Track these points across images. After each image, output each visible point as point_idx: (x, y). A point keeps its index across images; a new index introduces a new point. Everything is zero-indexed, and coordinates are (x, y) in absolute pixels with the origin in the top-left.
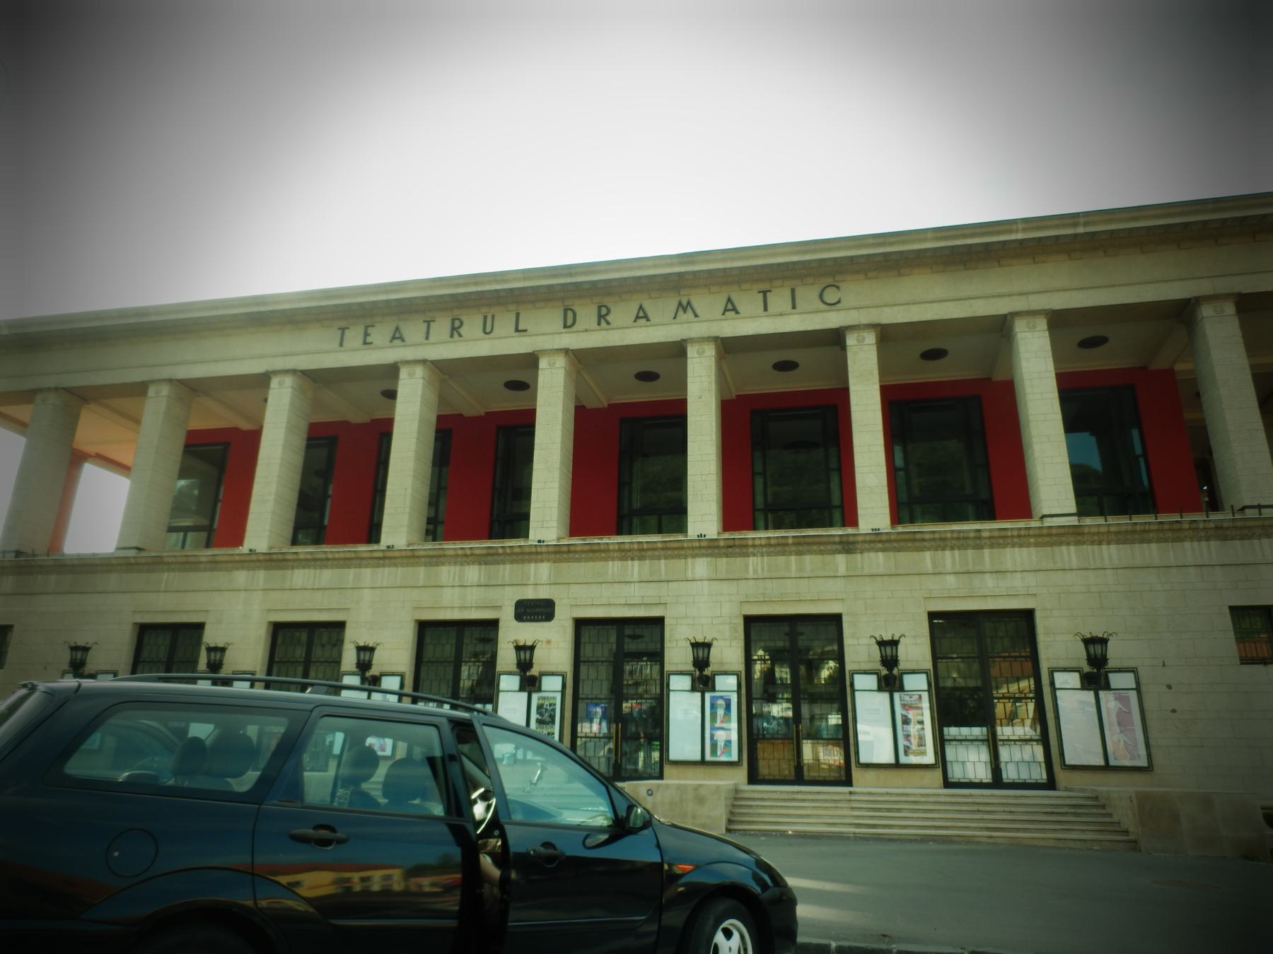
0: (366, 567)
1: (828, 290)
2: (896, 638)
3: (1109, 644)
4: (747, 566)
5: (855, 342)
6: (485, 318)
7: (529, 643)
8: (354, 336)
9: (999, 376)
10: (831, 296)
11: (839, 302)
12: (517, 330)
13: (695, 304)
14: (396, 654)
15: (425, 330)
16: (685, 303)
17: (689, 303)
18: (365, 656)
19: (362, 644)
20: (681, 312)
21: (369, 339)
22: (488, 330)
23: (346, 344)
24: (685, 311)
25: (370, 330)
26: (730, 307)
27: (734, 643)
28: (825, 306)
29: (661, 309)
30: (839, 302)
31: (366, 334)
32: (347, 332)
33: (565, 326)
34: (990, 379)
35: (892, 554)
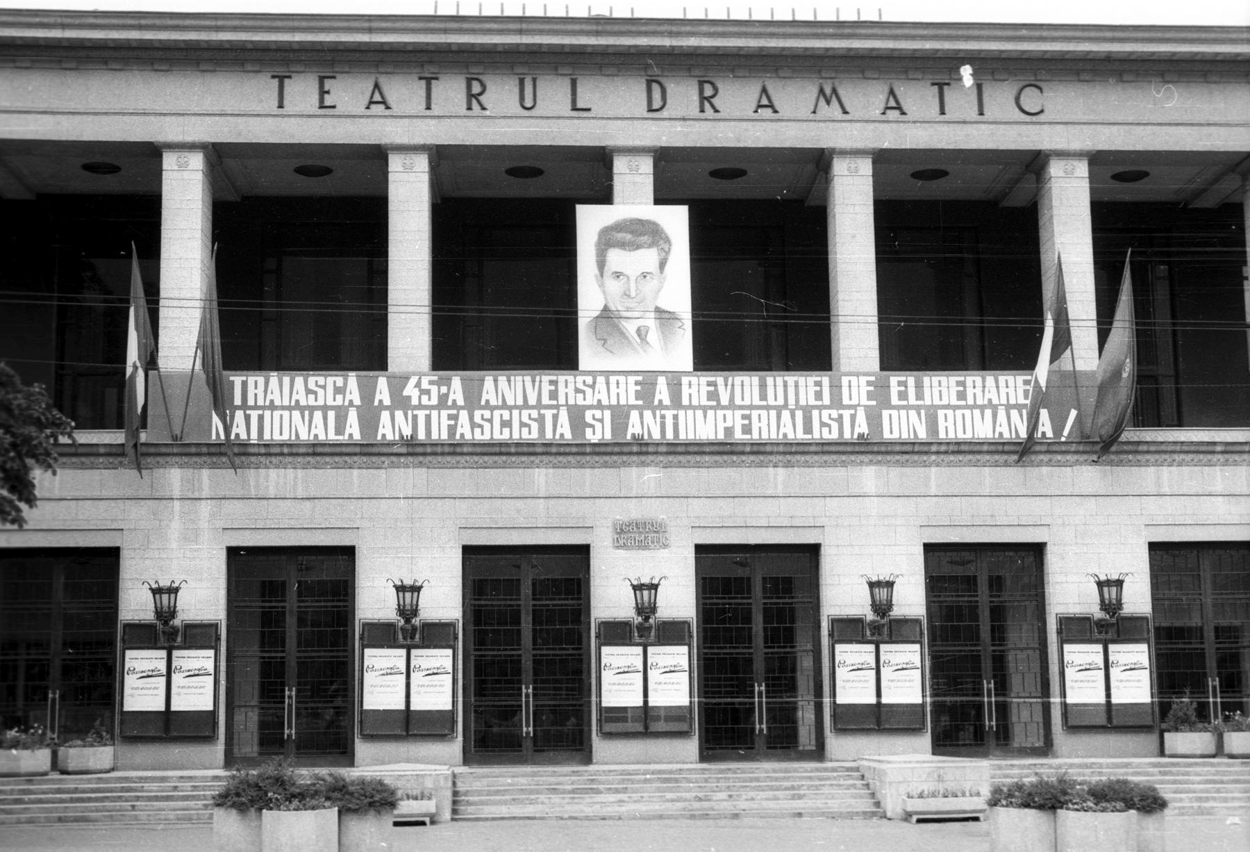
0: (172, 466)
1: (1028, 89)
2: (655, 582)
3: (1125, 585)
4: (928, 478)
5: (1061, 174)
6: (522, 82)
7: (1115, 577)
8: (302, 91)
9: (812, 202)
10: (1031, 100)
11: (1042, 111)
12: (574, 109)
13: (841, 92)
14: (205, 598)
15: (423, 93)
16: (828, 91)
17: (834, 91)
18: (882, 594)
19: (874, 579)
20: (822, 102)
21: (328, 100)
22: (528, 104)
23: (289, 108)
24: (828, 102)
25: (328, 84)
26: (892, 103)
27: (912, 580)
28: (1028, 118)
29: (795, 97)
30: (1042, 111)
31: (323, 93)
32: (287, 81)
33: (650, 110)
34: (801, 201)
35: (884, 469)
